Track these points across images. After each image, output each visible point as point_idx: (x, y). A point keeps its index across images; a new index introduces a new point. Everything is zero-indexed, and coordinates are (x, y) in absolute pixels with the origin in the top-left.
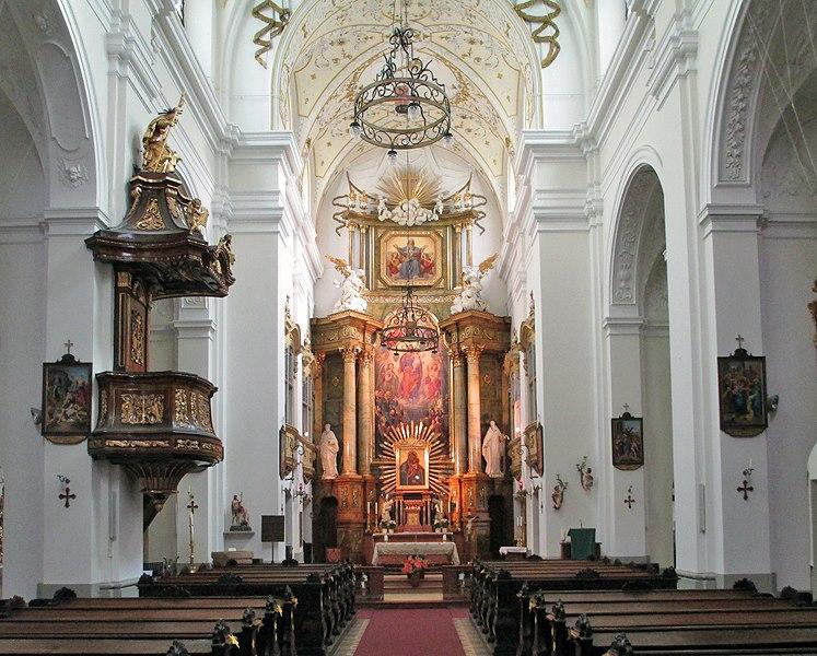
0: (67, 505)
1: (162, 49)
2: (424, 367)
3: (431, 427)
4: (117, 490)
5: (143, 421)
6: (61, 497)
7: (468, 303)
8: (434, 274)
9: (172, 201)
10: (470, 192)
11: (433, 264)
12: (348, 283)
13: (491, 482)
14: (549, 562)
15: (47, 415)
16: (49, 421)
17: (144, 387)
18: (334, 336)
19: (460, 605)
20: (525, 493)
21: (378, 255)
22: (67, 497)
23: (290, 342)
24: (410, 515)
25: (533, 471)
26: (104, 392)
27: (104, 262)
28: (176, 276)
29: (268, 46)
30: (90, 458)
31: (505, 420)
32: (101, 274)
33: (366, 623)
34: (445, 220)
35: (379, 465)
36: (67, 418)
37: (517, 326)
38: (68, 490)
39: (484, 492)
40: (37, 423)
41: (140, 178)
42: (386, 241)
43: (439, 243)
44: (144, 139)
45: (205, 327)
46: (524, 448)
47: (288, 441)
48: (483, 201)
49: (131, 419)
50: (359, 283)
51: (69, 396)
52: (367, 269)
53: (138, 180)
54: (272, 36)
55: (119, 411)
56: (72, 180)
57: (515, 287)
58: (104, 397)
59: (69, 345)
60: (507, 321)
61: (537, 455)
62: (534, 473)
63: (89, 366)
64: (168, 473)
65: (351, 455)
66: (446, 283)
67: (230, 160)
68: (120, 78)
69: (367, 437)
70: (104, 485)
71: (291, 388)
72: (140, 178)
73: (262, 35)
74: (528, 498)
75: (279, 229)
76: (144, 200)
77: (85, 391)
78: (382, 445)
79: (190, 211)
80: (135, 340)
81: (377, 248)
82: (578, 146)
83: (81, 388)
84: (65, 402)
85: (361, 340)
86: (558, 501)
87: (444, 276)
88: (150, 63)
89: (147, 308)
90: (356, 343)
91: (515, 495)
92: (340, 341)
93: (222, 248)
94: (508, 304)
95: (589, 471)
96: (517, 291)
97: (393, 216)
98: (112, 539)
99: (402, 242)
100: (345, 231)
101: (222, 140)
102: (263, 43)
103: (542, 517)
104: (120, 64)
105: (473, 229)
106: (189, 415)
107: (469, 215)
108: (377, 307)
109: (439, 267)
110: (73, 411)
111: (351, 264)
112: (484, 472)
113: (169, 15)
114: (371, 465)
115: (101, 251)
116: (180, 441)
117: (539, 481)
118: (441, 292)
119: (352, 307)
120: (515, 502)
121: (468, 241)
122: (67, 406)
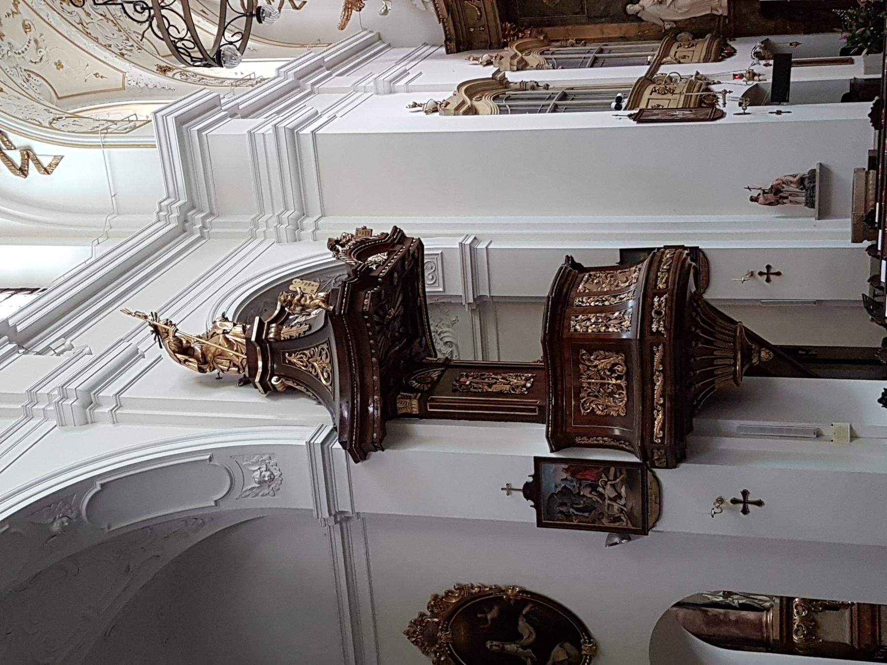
0: (759, 503)
1: (66, 336)
4: (735, 424)
5: (623, 383)
6: (745, 511)
9: (286, 332)
15: (617, 525)
16: (625, 523)
17: (569, 382)
22: (745, 502)
26: (578, 440)
27: (384, 433)
28: (397, 324)
29: (28, 154)
30: (683, 465)
32: (400, 439)
36: (619, 496)
38: (735, 501)
40: (629, 539)
41: (257, 379)
44: (201, 370)
45: (470, 253)
49: (618, 405)
51: (586, 492)
53: (260, 382)
54: (12, 147)
55: (607, 420)
56: (272, 479)
58: (585, 440)
59: (509, 489)
63: (539, 461)
64: (707, 342)
67: (211, 214)
68: (119, 406)
70: (727, 444)
72: (257, 379)
73: (14, 165)
75: (308, 130)
76: (289, 373)
77: (577, 467)
79: (298, 309)
80: (494, 389)
83: (573, 475)
84: (595, 498)
88: (87, 359)
89: (447, 364)
93: (348, 253)
98: (819, 435)
101: (183, 228)
102: (25, 162)
104: (98, 405)
106: (612, 309)
110: (608, 487)
113: (15, 326)
115: (369, 440)
116: (654, 327)
122: (601, 495)
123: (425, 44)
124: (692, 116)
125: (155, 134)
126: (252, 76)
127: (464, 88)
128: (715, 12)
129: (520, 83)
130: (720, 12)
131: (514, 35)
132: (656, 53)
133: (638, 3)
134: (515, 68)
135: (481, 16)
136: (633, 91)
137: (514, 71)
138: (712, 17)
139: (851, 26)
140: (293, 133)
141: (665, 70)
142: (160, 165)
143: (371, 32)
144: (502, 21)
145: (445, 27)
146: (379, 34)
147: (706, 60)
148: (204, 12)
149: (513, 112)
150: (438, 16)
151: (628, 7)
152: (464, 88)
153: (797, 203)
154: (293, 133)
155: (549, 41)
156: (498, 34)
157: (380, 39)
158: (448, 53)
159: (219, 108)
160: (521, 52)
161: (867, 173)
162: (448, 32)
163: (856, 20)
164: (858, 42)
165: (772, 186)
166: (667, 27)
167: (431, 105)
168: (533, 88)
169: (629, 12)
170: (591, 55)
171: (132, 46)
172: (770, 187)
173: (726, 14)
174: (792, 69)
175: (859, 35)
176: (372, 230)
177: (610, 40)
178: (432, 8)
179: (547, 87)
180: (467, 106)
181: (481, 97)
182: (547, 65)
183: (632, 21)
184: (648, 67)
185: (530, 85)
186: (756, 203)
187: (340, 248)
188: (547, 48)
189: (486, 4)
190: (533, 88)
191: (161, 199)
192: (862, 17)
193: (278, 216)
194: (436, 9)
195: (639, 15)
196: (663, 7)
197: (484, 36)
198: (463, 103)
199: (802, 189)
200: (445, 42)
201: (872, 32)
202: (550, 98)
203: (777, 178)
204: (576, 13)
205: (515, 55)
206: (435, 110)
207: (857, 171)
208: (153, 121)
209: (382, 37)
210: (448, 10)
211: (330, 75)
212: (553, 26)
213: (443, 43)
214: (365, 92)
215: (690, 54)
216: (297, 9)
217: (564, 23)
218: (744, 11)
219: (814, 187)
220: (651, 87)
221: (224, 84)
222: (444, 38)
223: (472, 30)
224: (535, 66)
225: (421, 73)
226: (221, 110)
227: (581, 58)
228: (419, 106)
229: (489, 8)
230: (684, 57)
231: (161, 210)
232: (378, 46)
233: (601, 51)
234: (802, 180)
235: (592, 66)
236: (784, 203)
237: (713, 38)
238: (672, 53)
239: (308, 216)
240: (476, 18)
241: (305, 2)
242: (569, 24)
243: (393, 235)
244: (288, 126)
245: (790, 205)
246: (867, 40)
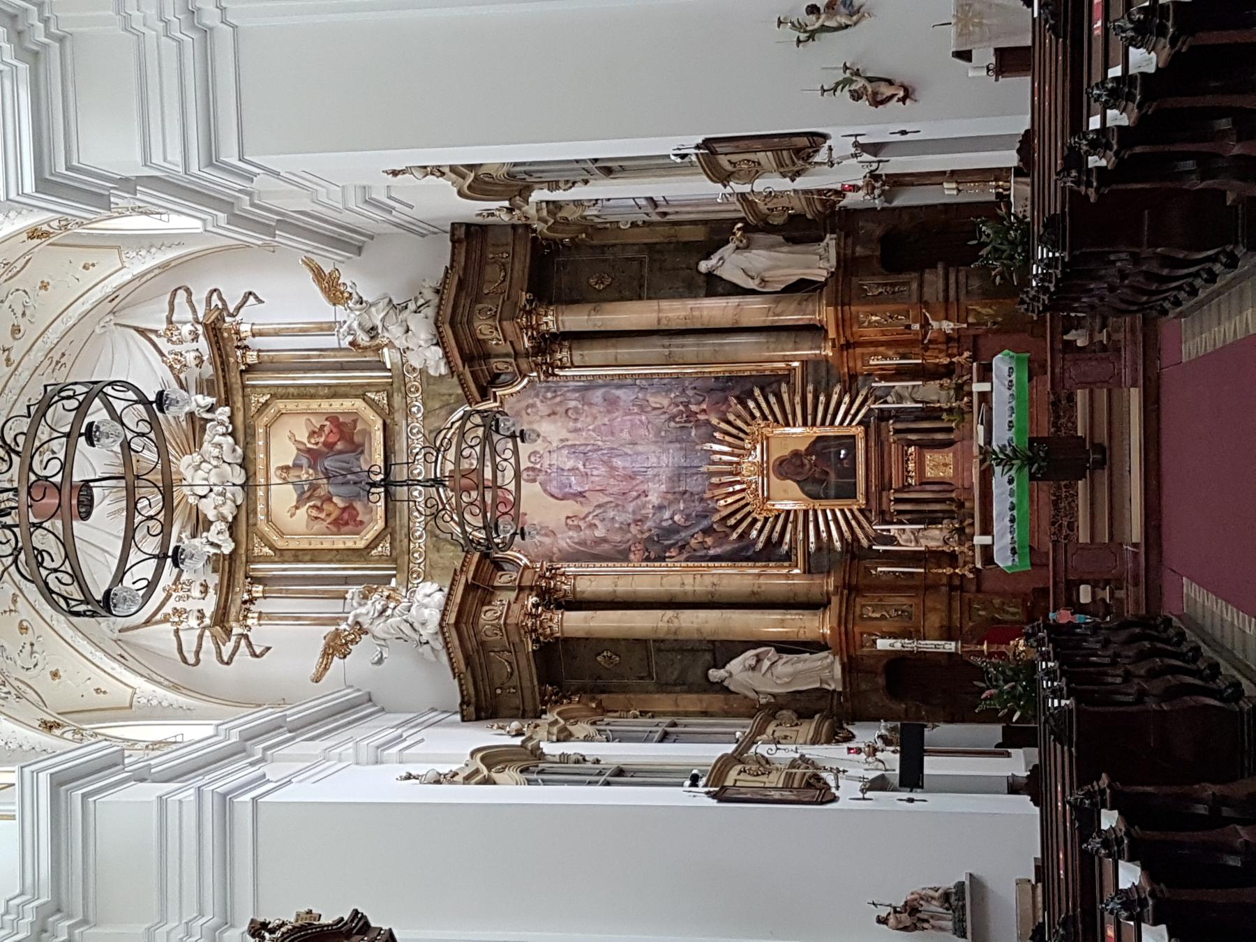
2: (574, 439)
3: (714, 421)
7: (421, 329)
8: (355, 417)
10: (162, 327)
11: (333, 418)
12: (379, 628)
13: (847, 267)
14: (1037, 111)
18: (501, 664)
19: (1151, 347)
20: (874, 176)
21: (315, 555)
23: (512, 774)
24: (929, 473)
25: (817, 159)
31: (699, 234)
33: (1191, 589)
34: (227, 387)
35: (807, 554)
37: (472, 210)
39: (872, 285)
42: (281, 534)
43: (280, 405)
46: (760, 185)
47: (747, 781)
48: (182, 295)
50: (375, 602)
52: (347, 580)
57: (379, 215)
60: (461, 233)
61: (776, 151)
62: (822, 156)
65: (782, 623)
66: (377, 388)
67: (85, 921)
69: (746, 582)
71: (620, 772)
74: (885, 170)
78: (760, 545)
81: (298, 555)
82: (35, 57)
85: (513, 595)
86: (886, 91)
87: (360, 392)
90: (516, 608)
91: (878, 203)
92: (514, 648)
94: (419, 230)
95: (813, 9)
96: (389, 210)
97: (224, 519)
99: (282, 497)
100: (260, 634)
103: (928, 131)
105: (247, 321)
107: (214, 331)
108: (434, 556)
109: (337, 405)
111: (334, 621)
112: (822, 286)
114: (808, 571)
117: (840, 143)
118: (397, 399)
119: (432, 616)
120: (897, 203)
121: (277, 333)
123: (433, 710)
124: (793, 798)
125: (17, 799)
126: (179, 739)
127: (480, 755)
128: (826, 686)
129: (560, 756)
130: (833, 687)
131: (556, 702)
132: (748, 731)
133: (723, 667)
134: (554, 738)
135: (512, 674)
136: (712, 771)
137: (552, 742)
138: (821, 693)
139: (997, 680)
140: (225, 800)
141: (762, 749)
142: (17, 845)
143: (359, 690)
144: (541, 683)
145: (461, 685)
146: (369, 694)
147: (814, 742)
148: (123, 657)
149: (545, 782)
150: (453, 669)
151: (711, 672)
152: (480, 755)
153: (941, 929)
154: (225, 800)
155: (604, 710)
156: (534, 699)
157: (370, 700)
158: (463, 720)
159: (121, 767)
160: (566, 720)
161: (1034, 888)
162: (465, 693)
163: (1003, 673)
164: (1007, 701)
165: (906, 902)
166: (763, 701)
167: (432, 776)
168: (577, 762)
169: (712, 679)
170: (660, 729)
171: (9, 693)
172: (902, 903)
173: (840, 689)
174: (926, 758)
175: (1008, 693)
176: (320, 916)
177: (687, 714)
178: (445, 658)
179: (598, 761)
180: (482, 776)
181: (504, 769)
182: (598, 737)
183: (716, 692)
184: (734, 746)
185: (573, 758)
186: (885, 926)
187: (267, 935)
188: (600, 718)
189: (519, 657)
190: (577, 762)
191: (11, 895)
192: (1011, 669)
193: (187, 923)
194: (450, 659)
195: (726, 683)
196: (756, 674)
197: (517, 702)
198: (477, 771)
199: (947, 909)
200: (461, 705)
201: (1024, 688)
202: (600, 774)
203: (913, 890)
204: (642, 678)
205: (555, 722)
206: (438, 782)
207: (1019, 883)
208: (17, 786)
209: (374, 698)
210: (467, 664)
211: (293, 738)
212: (610, 692)
213: (458, 709)
214: (340, 761)
215: (793, 735)
216: (257, 656)
217: (624, 690)
218: (863, 686)
219: (963, 906)
220: (739, 767)
221: (136, 747)
222: (459, 700)
223: (499, 691)
224: (582, 737)
225: (423, 740)
226: (123, 770)
227: (645, 732)
228: (415, 778)
229: (523, 663)
230: (786, 737)
231: (7, 912)
232: (365, 709)
233: (674, 725)
234: (946, 896)
235: (661, 740)
236: (924, 929)
237: (824, 719)
238: (770, 730)
239: (232, 926)
240: (506, 674)
241: (268, 649)
242: (630, 692)
243: (352, 921)
244: (218, 790)
245: (933, 932)
246: (1020, 697)
